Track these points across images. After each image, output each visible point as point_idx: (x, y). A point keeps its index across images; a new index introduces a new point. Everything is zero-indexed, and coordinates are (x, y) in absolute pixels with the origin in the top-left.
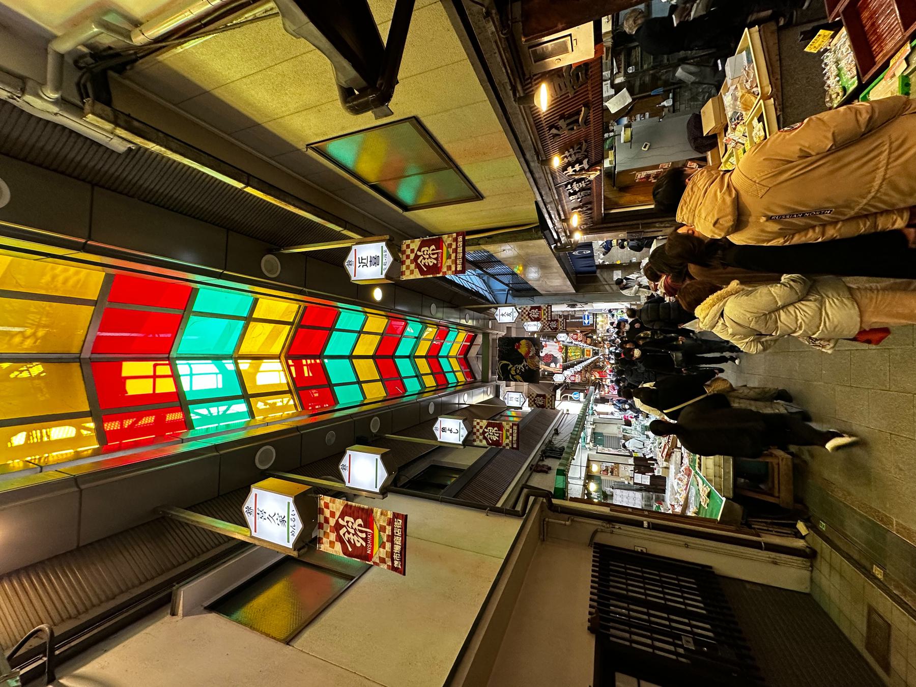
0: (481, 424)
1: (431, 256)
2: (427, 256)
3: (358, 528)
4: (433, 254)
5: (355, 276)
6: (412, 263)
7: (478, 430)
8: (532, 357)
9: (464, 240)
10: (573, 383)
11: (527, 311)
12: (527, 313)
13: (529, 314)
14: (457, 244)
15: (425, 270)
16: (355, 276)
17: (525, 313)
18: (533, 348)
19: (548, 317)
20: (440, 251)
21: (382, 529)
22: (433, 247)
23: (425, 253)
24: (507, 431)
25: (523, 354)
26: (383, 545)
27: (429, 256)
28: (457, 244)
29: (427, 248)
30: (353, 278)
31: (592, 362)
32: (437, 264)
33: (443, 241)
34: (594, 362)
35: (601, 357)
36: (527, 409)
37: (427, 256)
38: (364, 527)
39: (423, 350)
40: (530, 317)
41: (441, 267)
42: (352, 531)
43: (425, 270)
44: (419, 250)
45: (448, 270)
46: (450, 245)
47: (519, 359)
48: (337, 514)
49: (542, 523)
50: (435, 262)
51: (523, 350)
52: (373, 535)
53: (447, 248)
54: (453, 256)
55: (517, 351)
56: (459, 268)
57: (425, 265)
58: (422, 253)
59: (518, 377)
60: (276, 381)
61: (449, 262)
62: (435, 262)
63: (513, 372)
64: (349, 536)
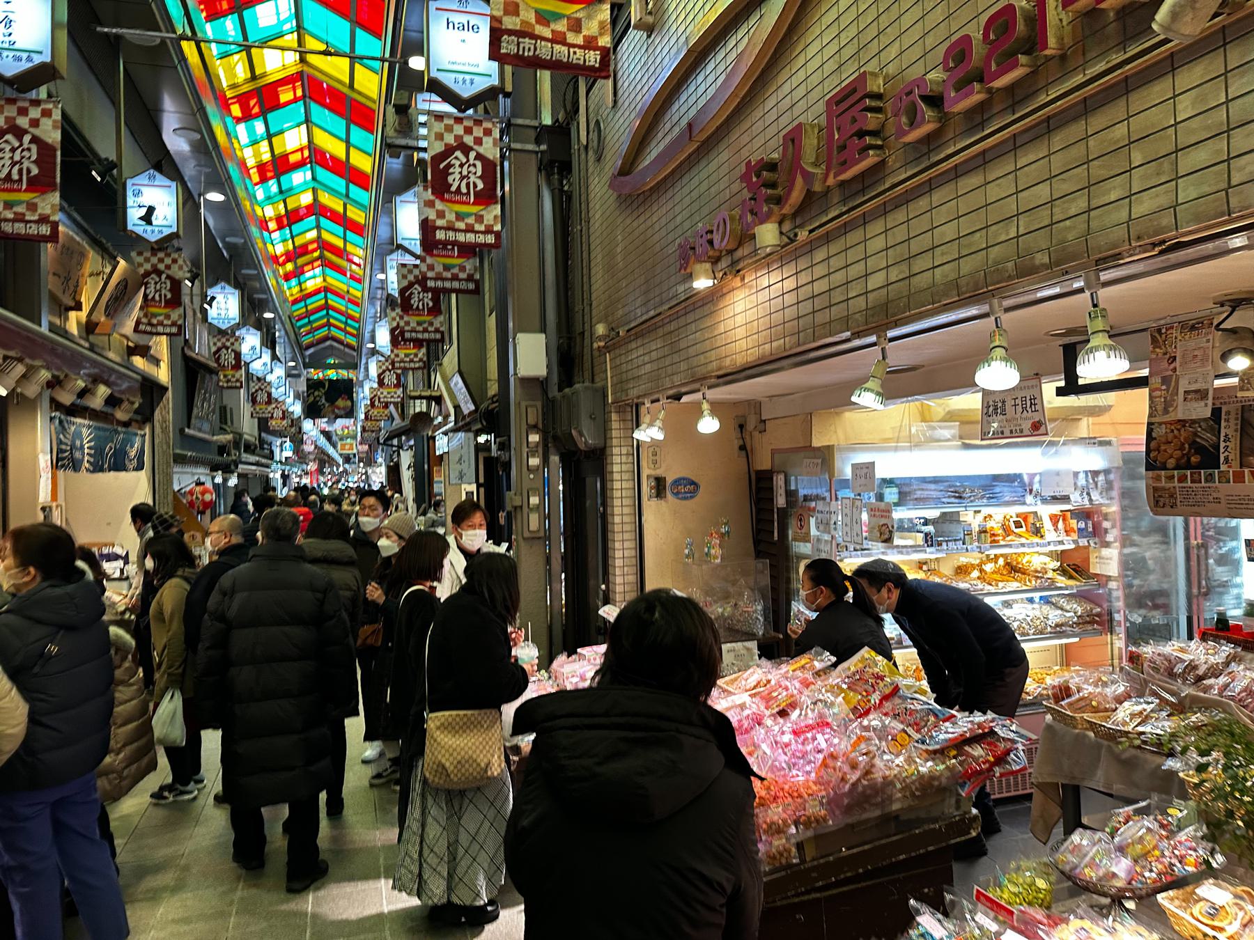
0: (46, 123)
1: (17, 168)
2: (465, 173)
3: (25, 166)
4: (468, 185)
5: (437, 9)
6: (457, 138)
7: (161, 260)
8: (333, 412)
9: (397, 403)
10: (302, 442)
11: (168, 267)
12: (469, 140)
13: (466, 150)
14: (580, 47)
15: (442, 166)
16: (437, 9)
17: (468, 131)
18: (342, 412)
19: (439, 278)
20: (472, 200)
21: (168, 317)
22: (480, 186)
23: (471, 168)
24: (480, 219)
25: (337, 403)
26: (419, 324)
27: (16, 163)
28: (580, 47)
29: (479, 173)
30: (398, 199)
31: (328, 456)
32: (448, 191)
33: (436, 316)
34: (331, 461)
35: (341, 469)
36: (813, 615)
37: (465, 173)
38: (28, 178)
39: (326, 199)
40: (449, 151)
41: (408, 315)
42: (158, 287)
43: (442, 166)
44: (479, 157)
45: (428, 266)
46: (463, 269)
47: (332, 399)
48: (170, 272)
49: (859, 553)
50: (453, 189)
51: (341, 403)
52: (20, 190)
53: (476, 215)
54: (461, 225)
55: (340, 396)
56: (431, 284)
57: (411, 293)
58: (471, 162)
59: (312, 399)
60: (233, 22)
61: (439, 268)
62: (453, 189)
63: (316, 393)
64: (457, 165)
